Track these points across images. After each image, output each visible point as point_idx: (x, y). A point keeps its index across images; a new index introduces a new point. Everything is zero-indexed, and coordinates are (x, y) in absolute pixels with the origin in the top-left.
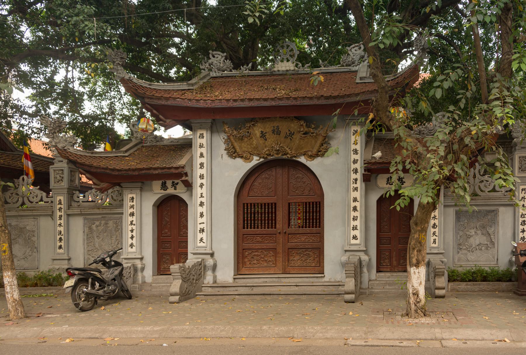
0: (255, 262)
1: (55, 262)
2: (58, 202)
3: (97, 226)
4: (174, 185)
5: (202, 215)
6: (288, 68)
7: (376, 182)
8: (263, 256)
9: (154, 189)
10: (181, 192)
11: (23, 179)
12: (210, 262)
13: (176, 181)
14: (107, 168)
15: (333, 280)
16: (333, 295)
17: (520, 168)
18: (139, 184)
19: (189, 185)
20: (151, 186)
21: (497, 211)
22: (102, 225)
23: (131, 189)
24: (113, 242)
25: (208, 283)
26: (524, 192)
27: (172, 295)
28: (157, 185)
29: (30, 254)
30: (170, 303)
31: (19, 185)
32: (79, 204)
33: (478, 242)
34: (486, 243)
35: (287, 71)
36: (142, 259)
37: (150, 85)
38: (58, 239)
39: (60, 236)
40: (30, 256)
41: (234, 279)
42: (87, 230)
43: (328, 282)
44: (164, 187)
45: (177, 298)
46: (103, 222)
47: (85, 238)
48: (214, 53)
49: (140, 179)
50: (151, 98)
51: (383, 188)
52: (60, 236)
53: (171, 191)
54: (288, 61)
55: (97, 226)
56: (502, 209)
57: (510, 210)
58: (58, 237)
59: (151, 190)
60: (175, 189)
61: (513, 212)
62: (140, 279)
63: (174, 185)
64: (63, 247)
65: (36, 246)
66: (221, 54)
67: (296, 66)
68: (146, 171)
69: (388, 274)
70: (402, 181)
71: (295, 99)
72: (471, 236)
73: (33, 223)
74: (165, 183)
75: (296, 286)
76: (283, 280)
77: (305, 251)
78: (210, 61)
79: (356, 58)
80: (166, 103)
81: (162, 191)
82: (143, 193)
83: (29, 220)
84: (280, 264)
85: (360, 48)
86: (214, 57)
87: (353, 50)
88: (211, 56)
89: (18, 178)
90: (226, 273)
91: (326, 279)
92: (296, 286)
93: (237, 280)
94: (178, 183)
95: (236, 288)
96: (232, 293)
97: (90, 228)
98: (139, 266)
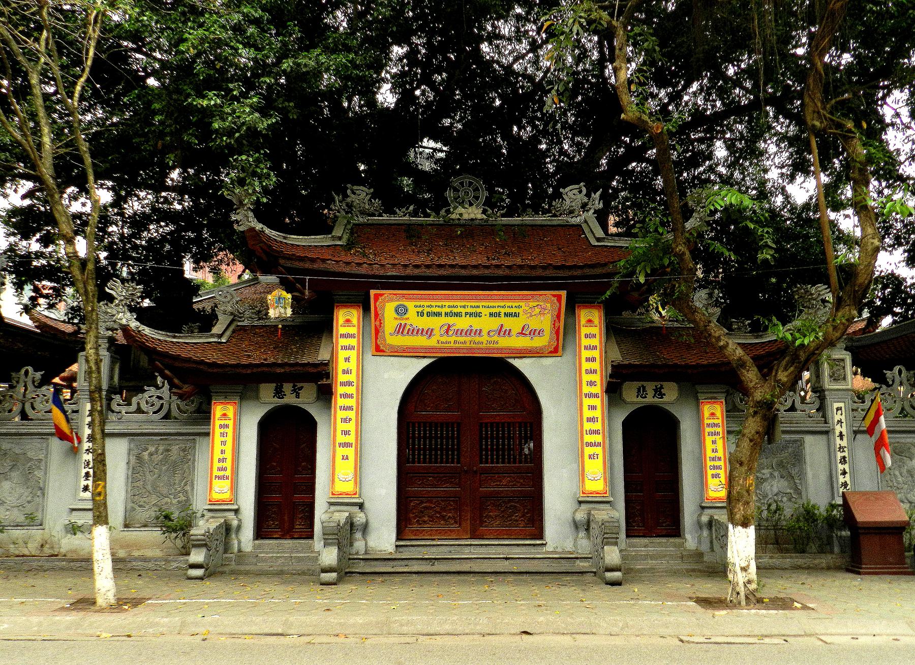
0: (426, 519)
1: (74, 513)
2: (88, 413)
3: (151, 454)
4: (296, 392)
5: (844, 473)
6: (472, 216)
7: (621, 394)
8: (438, 509)
9: (261, 396)
10: (306, 400)
11: (27, 372)
12: (360, 518)
13: (299, 385)
14: (202, 362)
15: (559, 550)
16: (566, 572)
17: (831, 377)
18: (240, 388)
19: (326, 394)
20: (257, 391)
21: (801, 443)
22: (160, 451)
23: (226, 396)
24: (177, 482)
25: (357, 553)
26: (839, 412)
27: (325, 571)
28: (267, 391)
29: (29, 499)
30: (322, 584)
31: (18, 382)
32: (119, 416)
33: (775, 490)
34: (789, 491)
35: (472, 220)
36: (236, 511)
37: (285, 238)
38: (83, 474)
39: (87, 470)
40: (29, 502)
41: (397, 546)
42: (133, 459)
43: (552, 552)
44: (279, 393)
45: (334, 575)
46: (161, 448)
47: (130, 473)
48: (355, 187)
49: (240, 382)
50: (292, 259)
51: (633, 403)
52: (87, 470)
53: (290, 399)
54: (471, 205)
55: (151, 454)
56: (808, 439)
57: (822, 439)
58: (84, 471)
59: (257, 398)
60: (298, 396)
61: (825, 443)
62: (236, 545)
63: (296, 392)
64: (90, 487)
65: (41, 485)
66: (366, 189)
67: (484, 212)
68: (265, 369)
69: (645, 541)
70: (661, 392)
71: (509, 267)
72: (765, 480)
73: (39, 445)
74: (282, 386)
75: (507, 559)
76: (467, 550)
77: (510, 501)
78: (349, 200)
79: (576, 205)
80: (311, 267)
81: (276, 399)
82: (244, 403)
83: (34, 441)
84: (467, 524)
85: (580, 192)
86: (354, 193)
87: (570, 194)
88: (349, 192)
89: (19, 371)
90: (383, 537)
91: (549, 548)
92: (507, 559)
93: (401, 549)
94: (302, 387)
95: (406, 562)
96: (400, 570)
97: (139, 458)
98: (235, 523)
